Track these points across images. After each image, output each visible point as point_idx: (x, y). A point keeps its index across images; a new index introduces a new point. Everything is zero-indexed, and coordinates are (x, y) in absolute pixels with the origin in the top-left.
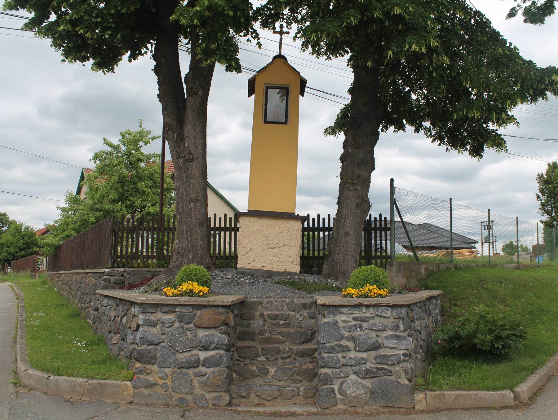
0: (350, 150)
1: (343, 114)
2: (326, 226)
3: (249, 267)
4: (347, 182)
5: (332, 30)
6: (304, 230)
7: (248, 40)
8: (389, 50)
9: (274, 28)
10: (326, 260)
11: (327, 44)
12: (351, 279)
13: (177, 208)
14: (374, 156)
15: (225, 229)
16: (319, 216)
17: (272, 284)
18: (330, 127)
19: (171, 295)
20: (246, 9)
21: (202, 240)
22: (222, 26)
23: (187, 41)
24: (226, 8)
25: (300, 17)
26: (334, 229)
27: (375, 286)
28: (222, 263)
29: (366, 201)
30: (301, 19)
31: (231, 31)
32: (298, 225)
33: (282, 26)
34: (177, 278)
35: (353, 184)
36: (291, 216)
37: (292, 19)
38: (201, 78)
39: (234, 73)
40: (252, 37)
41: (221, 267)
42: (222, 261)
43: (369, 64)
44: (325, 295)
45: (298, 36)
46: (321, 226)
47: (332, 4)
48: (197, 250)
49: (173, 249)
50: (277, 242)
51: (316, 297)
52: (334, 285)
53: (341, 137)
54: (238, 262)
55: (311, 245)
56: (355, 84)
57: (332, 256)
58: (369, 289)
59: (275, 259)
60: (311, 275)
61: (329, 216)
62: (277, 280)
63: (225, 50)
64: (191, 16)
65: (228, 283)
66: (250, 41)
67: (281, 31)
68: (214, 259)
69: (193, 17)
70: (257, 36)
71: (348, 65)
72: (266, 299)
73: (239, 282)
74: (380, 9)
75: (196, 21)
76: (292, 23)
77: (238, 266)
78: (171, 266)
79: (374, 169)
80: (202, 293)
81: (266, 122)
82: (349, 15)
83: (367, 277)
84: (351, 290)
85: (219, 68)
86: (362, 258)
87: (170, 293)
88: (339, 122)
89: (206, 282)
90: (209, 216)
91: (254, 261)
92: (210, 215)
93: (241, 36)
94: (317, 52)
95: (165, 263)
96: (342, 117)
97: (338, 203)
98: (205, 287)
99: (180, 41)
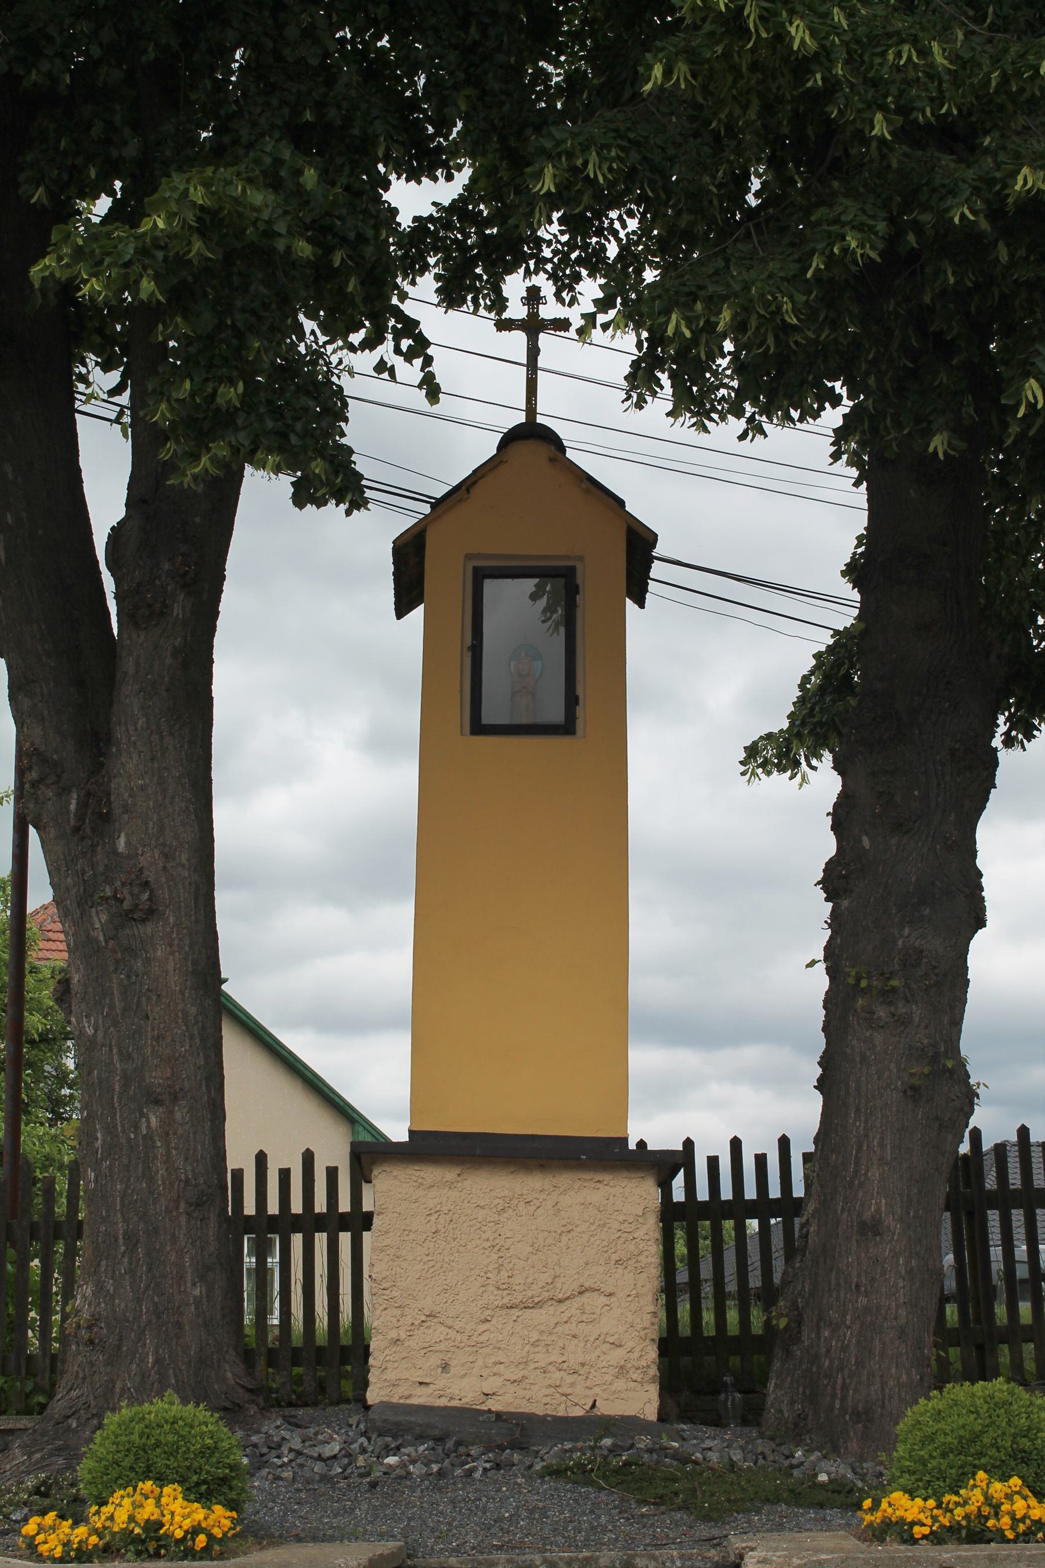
0: (866, 842)
1: (826, 677)
2: (775, 1192)
3: (421, 1397)
4: (856, 990)
5: (762, 296)
6: (670, 1214)
7: (381, 367)
8: (1027, 375)
9: (499, 304)
10: (778, 1352)
11: (739, 367)
12: (901, 1450)
13: (86, 1133)
14: (979, 863)
15: (310, 1223)
16: (736, 1145)
17: (529, 1479)
18: (769, 736)
19: (58, 1552)
20: (370, 233)
21: (202, 1278)
22: (266, 306)
23: (114, 377)
24: (281, 227)
25: (612, 250)
26: (811, 1207)
27: (1015, 1481)
28: (299, 1381)
29: (951, 1072)
30: (619, 257)
31: (309, 325)
32: (640, 1195)
33: (533, 296)
34: (85, 1468)
35: (888, 995)
36: (610, 1155)
37: (579, 261)
38: (183, 545)
39: (333, 511)
40: (398, 351)
41: (290, 1402)
42: (297, 1370)
43: (938, 444)
44: (780, 1528)
45: (601, 319)
46: (750, 1193)
47: (756, 184)
48: (179, 1325)
49: (72, 1321)
50: (546, 1277)
51: (737, 1543)
52: (823, 1477)
53: (823, 781)
54: (371, 1377)
55: (706, 1270)
56: (871, 538)
57: (807, 1336)
58: (988, 1498)
59: (542, 1358)
60: (710, 1431)
61: (784, 1143)
62: (551, 1460)
63: (277, 413)
64: (128, 265)
65: (325, 1478)
66: (392, 371)
67: (533, 315)
68: (261, 1362)
69: (137, 268)
70: (419, 348)
71: (836, 456)
72: (503, 1557)
73: (377, 1474)
74: (976, 191)
75: (147, 286)
76: (577, 278)
77: (372, 1396)
78: (58, 1407)
79: (981, 923)
80: (201, 1540)
81: (479, 728)
82: (837, 221)
83: (976, 1437)
84: (902, 1505)
85: (263, 493)
86: (945, 1336)
87: (51, 1544)
88: (811, 713)
89: (224, 1480)
90: (231, 1164)
91: (445, 1367)
92: (239, 1156)
93: (352, 348)
94: (695, 403)
95: (37, 1389)
96: (822, 689)
97: (822, 1085)
98: (219, 1509)
99: (84, 379)
